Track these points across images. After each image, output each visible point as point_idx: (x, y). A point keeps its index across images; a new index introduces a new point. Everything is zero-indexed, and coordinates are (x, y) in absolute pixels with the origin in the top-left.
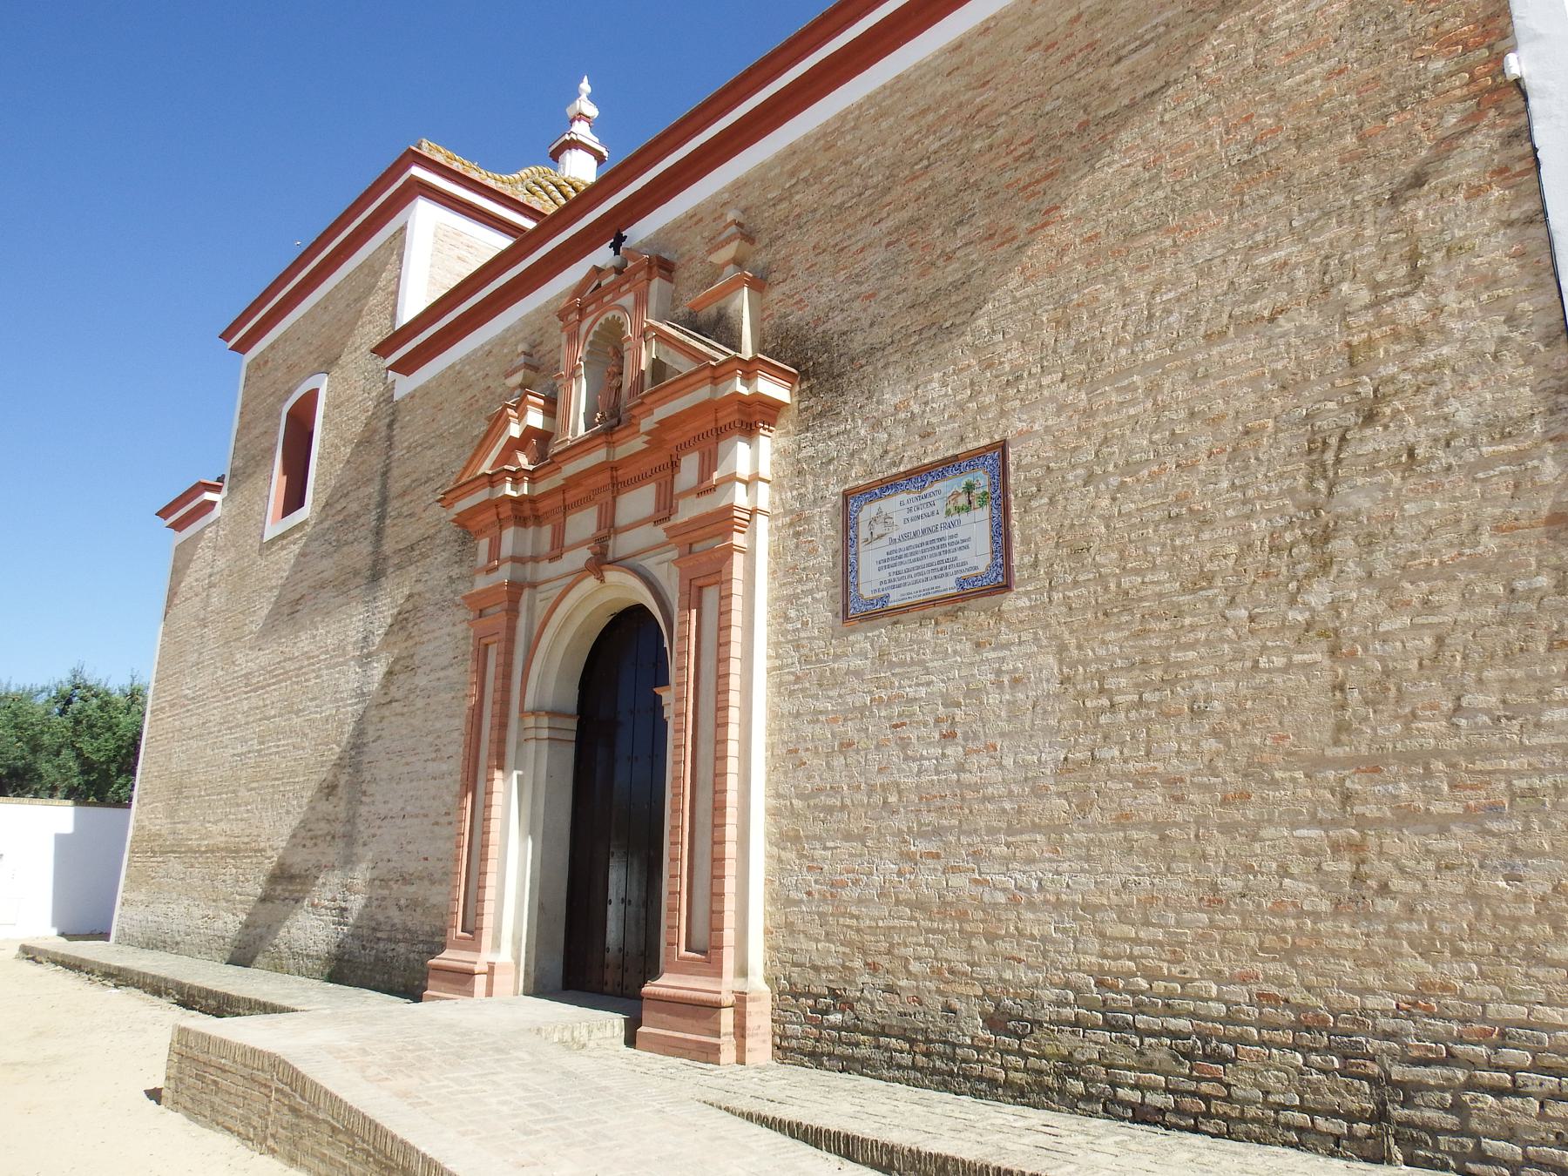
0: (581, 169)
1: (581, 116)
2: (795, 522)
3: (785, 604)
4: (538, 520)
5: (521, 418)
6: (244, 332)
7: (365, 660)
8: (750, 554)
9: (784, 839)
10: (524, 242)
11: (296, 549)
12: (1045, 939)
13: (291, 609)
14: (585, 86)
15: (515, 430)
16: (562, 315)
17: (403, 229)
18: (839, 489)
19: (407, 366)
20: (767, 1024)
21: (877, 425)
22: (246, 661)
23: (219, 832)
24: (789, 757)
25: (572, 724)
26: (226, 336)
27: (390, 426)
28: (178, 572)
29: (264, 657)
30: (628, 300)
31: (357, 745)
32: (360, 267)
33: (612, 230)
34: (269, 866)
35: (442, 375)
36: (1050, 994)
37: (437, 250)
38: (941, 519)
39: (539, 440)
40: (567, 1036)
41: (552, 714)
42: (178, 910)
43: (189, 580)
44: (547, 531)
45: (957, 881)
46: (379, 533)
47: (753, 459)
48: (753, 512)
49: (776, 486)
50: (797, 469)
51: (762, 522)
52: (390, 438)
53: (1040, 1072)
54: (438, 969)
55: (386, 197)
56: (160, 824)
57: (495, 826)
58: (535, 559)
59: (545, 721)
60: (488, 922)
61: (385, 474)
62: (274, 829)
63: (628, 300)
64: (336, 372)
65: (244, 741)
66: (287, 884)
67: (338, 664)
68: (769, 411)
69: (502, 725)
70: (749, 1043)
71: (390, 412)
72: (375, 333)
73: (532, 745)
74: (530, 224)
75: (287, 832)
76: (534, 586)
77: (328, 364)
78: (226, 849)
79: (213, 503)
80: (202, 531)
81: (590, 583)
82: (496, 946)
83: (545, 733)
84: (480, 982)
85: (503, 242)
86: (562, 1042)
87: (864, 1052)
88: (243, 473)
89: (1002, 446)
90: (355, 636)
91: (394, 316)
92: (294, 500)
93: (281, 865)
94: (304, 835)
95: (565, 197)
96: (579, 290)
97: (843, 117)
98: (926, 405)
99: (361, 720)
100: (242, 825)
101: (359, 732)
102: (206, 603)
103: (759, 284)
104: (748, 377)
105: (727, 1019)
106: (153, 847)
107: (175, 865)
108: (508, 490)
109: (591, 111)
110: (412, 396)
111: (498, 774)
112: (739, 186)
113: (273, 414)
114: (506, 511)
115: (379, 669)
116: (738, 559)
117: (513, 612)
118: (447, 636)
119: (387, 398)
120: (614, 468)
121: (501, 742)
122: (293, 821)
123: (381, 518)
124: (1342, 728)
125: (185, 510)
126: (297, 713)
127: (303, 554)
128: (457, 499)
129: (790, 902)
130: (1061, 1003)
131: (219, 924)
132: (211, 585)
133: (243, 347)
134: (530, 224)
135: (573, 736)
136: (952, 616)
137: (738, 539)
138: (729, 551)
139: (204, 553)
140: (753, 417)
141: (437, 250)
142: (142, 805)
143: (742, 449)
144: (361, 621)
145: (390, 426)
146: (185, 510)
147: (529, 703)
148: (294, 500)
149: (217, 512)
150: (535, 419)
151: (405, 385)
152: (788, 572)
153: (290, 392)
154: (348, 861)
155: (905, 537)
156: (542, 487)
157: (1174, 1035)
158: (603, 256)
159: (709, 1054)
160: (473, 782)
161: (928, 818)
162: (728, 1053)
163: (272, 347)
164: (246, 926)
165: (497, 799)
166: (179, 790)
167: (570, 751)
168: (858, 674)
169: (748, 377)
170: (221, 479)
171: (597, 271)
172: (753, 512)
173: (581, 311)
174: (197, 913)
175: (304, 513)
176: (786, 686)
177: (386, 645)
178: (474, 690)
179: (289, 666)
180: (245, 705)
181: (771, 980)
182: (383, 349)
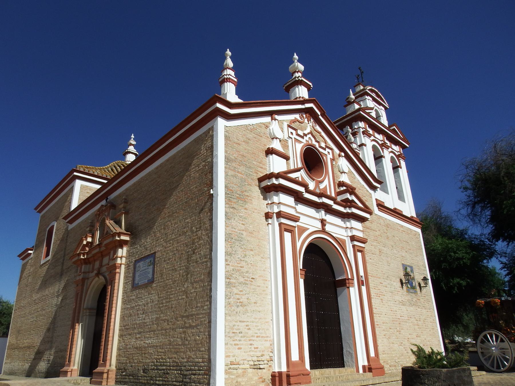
0: (130, 158)
1: (131, 144)
2: (128, 266)
3: (125, 283)
4: (90, 263)
5: (86, 239)
6: (40, 208)
7: (58, 297)
8: (120, 273)
9: (121, 336)
10: (104, 186)
11: (47, 267)
12: (151, 353)
13: (45, 283)
14: (133, 136)
15: (85, 243)
16: (96, 215)
17: (73, 186)
18: (134, 260)
19: (71, 222)
20: (114, 376)
21: (140, 246)
22: (35, 297)
23: (26, 342)
24: (123, 318)
25: (95, 311)
26: (36, 209)
27: (67, 237)
28: (22, 272)
29: (39, 296)
30: (106, 214)
31: (55, 318)
32: (65, 195)
33: (105, 196)
34: (36, 350)
35: (77, 225)
36: (150, 364)
37: (81, 191)
38: (146, 267)
39: (92, 243)
40: (75, 382)
41: (90, 309)
42: (17, 364)
43: (24, 274)
44: (91, 265)
45: (142, 342)
46: (63, 264)
47: (122, 252)
48: (121, 264)
49: (126, 258)
50: (130, 255)
51: (123, 267)
52: (67, 240)
53: (148, 380)
54: (62, 371)
55: (68, 181)
56: (14, 341)
57: (75, 336)
58: (89, 272)
59: (88, 311)
60: (72, 359)
61: (65, 249)
62: (37, 340)
63: (106, 214)
64: (58, 221)
65: (33, 318)
66: (39, 355)
67: (53, 297)
68: (125, 242)
69: (79, 312)
70: (109, 380)
71: (67, 233)
72: (65, 213)
73: (85, 317)
74: (105, 182)
75: (40, 341)
76: (88, 279)
77: (56, 219)
78: (28, 347)
79: (31, 253)
80: (28, 261)
81: (97, 279)
82: (74, 365)
83: (88, 314)
84: (69, 373)
85: (98, 187)
86: (74, 383)
87: (127, 380)
88: (37, 247)
89: (155, 253)
90: (56, 290)
91: (70, 208)
92: (47, 255)
93: (38, 350)
94: (43, 342)
95: (117, 171)
96: (99, 210)
97: (142, 178)
98: (147, 242)
99: (56, 312)
100: (31, 340)
101: (55, 315)
102: (28, 280)
103: (126, 213)
104: (119, 236)
105: (105, 376)
106: (13, 348)
107: (17, 352)
108: (82, 257)
109: (134, 143)
110: (71, 229)
111: (77, 324)
112: (127, 190)
113: (45, 230)
114: (82, 261)
115: (60, 299)
116: (117, 275)
117: (83, 285)
118: (72, 291)
119: (67, 229)
120: (102, 252)
121: (78, 316)
122: (41, 338)
123: (64, 260)
124: (186, 310)
125: (24, 255)
126: (44, 310)
127: (48, 268)
128: (73, 258)
129: (121, 349)
130: (152, 366)
131: (25, 367)
132: (29, 276)
133: (40, 212)
134: (105, 182)
135: (95, 314)
136: (146, 287)
137: (118, 270)
138: (116, 273)
139: (28, 267)
140: (122, 244)
141: (81, 191)
142: (10, 336)
143: (120, 250)
144: (58, 287)
145: (67, 237)
146: (24, 255)
147: (85, 307)
148: (47, 255)
149: (32, 256)
150: (89, 240)
151: (71, 227)
152: (126, 277)
153: (49, 225)
154: (51, 348)
155: (142, 271)
156: (89, 256)
157: (164, 370)
158: (104, 202)
159: (100, 383)
160: (73, 328)
161: (140, 330)
162: (104, 383)
163: (46, 212)
164: (30, 366)
165: (76, 330)
166: (19, 332)
167: (94, 318)
168: (133, 299)
169: (119, 236)
170: (33, 247)
171: (102, 206)
172: (121, 264)
173: (99, 215)
174: (20, 364)
175: (49, 258)
176: (124, 302)
177: (62, 292)
178: (75, 304)
179: (44, 298)
180: (34, 308)
181: (116, 367)
182: (65, 218)
